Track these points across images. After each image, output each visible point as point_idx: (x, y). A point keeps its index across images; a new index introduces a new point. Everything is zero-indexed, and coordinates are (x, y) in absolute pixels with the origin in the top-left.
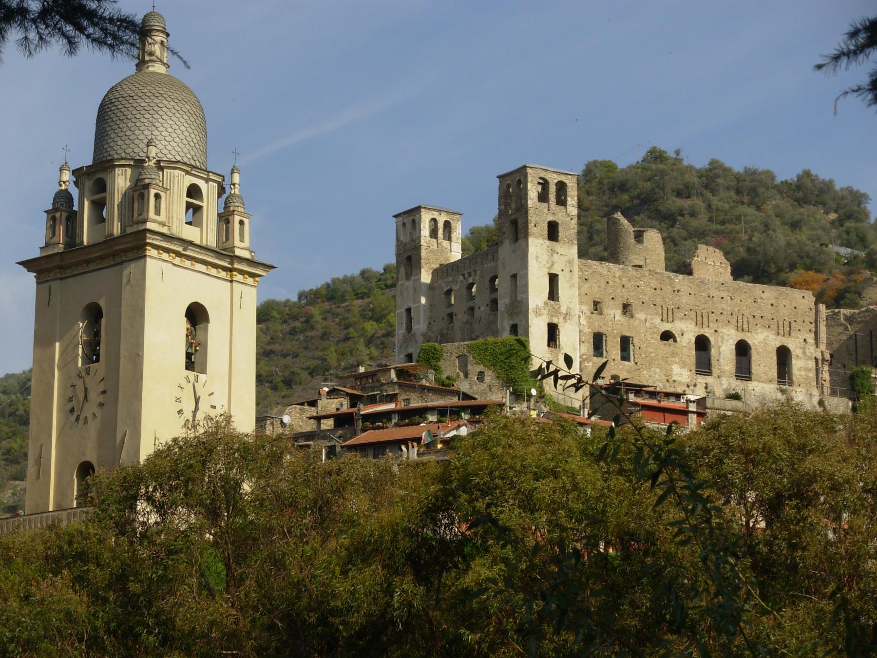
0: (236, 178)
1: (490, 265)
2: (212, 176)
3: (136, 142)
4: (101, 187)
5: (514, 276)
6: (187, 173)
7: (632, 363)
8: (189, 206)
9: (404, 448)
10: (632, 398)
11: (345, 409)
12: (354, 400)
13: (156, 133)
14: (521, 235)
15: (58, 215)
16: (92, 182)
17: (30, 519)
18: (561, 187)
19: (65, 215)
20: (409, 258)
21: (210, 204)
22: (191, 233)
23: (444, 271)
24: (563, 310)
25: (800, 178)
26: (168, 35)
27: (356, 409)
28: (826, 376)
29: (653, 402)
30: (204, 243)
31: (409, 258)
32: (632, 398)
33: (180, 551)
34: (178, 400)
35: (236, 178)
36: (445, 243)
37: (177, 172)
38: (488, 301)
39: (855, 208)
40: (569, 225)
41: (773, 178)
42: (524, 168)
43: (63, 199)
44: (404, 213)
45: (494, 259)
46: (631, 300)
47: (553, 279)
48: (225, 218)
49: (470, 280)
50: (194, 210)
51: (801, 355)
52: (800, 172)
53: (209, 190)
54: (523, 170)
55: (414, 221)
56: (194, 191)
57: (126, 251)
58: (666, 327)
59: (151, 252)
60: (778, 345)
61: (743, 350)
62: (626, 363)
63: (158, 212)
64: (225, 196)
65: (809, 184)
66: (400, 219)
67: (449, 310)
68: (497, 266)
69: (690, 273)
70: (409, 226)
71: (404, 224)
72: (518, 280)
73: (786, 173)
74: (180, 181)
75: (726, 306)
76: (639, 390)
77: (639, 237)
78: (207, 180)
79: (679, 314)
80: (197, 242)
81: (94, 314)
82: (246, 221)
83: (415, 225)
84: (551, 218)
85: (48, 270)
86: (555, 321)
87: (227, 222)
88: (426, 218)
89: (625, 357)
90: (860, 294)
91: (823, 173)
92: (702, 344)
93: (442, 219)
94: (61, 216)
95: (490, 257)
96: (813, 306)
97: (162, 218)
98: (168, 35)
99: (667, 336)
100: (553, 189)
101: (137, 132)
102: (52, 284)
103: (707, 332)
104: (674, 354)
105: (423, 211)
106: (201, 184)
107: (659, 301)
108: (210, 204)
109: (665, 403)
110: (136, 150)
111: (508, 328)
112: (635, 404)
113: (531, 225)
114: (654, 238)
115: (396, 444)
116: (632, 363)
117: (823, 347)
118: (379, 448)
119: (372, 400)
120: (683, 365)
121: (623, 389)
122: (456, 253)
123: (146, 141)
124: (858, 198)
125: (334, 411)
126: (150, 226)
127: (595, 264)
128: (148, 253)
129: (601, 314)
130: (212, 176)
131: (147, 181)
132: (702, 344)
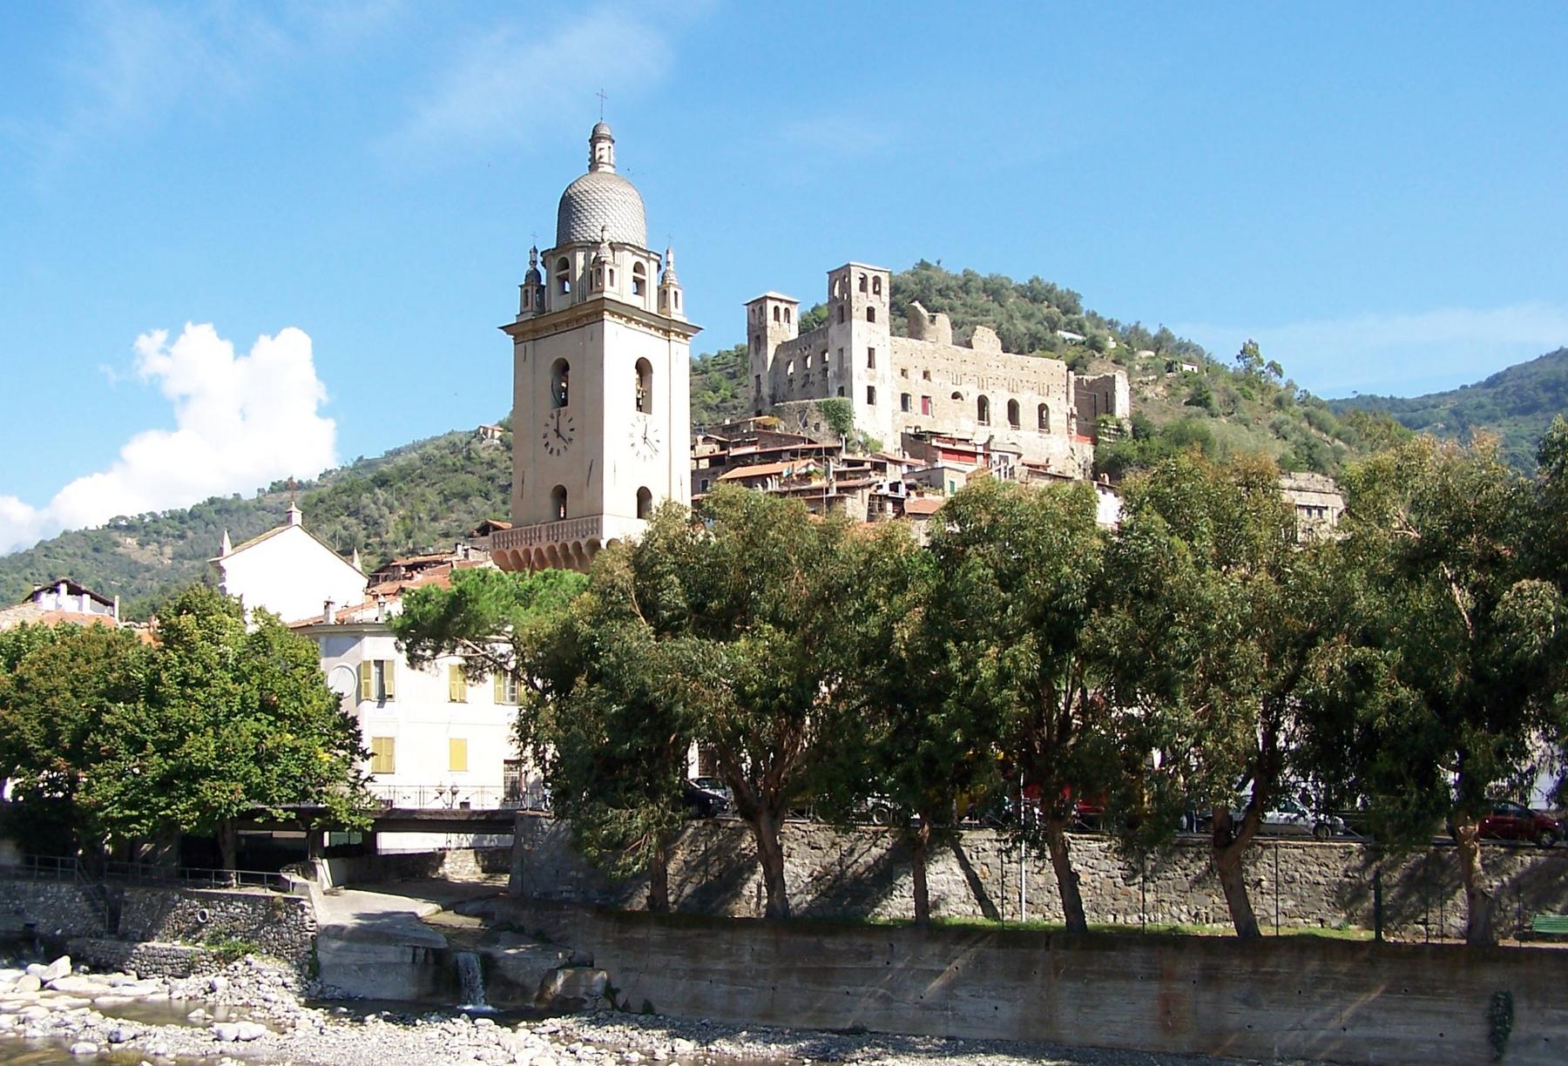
0: (671, 258)
1: (821, 341)
2: (652, 256)
3: (592, 228)
4: (565, 264)
5: (841, 350)
6: (634, 253)
7: (930, 416)
8: (635, 280)
9: (768, 480)
10: (934, 442)
11: (717, 452)
12: (723, 446)
13: (607, 220)
14: (846, 317)
15: (529, 288)
16: (557, 261)
17: (563, 524)
18: (877, 280)
19: (535, 288)
20: (758, 337)
21: (652, 278)
22: (637, 301)
23: (784, 347)
24: (879, 375)
25: (1031, 282)
26: (613, 142)
27: (726, 452)
28: (1074, 427)
29: (950, 446)
30: (647, 310)
31: (758, 337)
32: (934, 442)
33: (995, 521)
34: (631, 435)
35: (671, 258)
36: (785, 325)
37: (626, 252)
38: (820, 369)
39: (1072, 305)
40: (883, 312)
41: (1010, 283)
42: (849, 265)
43: (533, 276)
44: (753, 302)
45: (825, 336)
46: (929, 369)
47: (871, 351)
48: (663, 293)
49: (806, 353)
50: (640, 284)
51: (1056, 411)
52: (1031, 278)
53: (651, 268)
54: (847, 268)
55: (761, 308)
56: (638, 268)
57: (587, 316)
58: (956, 389)
59: (607, 316)
60: (1040, 403)
61: (1013, 408)
62: (926, 416)
63: (612, 284)
64: (661, 272)
65: (1039, 287)
66: (751, 306)
67: (806, 372)
68: (827, 343)
69: (972, 347)
70: (757, 311)
71: (754, 310)
72: (843, 354)
73: (1021, 279)
74: (627, 260)
75: (1001, 372)
76: (937, 435)
77: (933, 320)
78: (648, 259)
79: (965, 379)
80: (642, 308)
81: (562, 368)
82: (679, 292)
83: (762, 311)
84: (870, 305)
85: (523, 334)
86: (872, 384)
87: (665, 292)
88: (770, 305)
89: (925, 411)
90: (1085, 368)
91: (1048, 279)
92: (983, 403)
93: (870, 276)
94: (532, 290)
95: (821, 336)
96: (1065, 373)
97: (615, 288)
98: (613, 142)
99: (956, 396)
100: (870, 282)
101: (592, 220)
102: (527, 344)
103: (986, 393)
104: (961, 410)
105: (769, 302)
106: (643, 261)
107: (950, 370)
108: (652, 278)
109: (959, 447)
110: (592, 234)
111: (836, 390)
112: (938, 448)
113: (854, 310)
114: (943, 320)
115: (763, 479)
116: (930, 416)
117: (1072, 404)
118: (748, 481)
119: (737, 445)
120: (969, 417)
121: (928, 435)
122: (793, 334)
123: (600, 228)
124: (1075, 297)
125: (709, 454)
126: (605, 295)
127: (898, 338)
128: (605, 317)
129: (907, 378)
130: (652, 256)
131: (603, 259)
132: (983, 403)
